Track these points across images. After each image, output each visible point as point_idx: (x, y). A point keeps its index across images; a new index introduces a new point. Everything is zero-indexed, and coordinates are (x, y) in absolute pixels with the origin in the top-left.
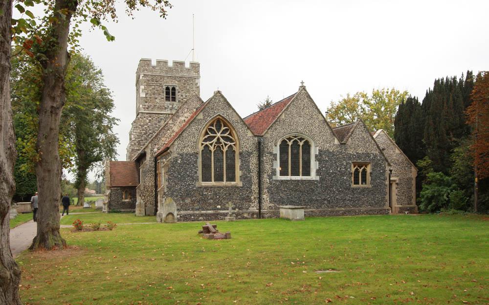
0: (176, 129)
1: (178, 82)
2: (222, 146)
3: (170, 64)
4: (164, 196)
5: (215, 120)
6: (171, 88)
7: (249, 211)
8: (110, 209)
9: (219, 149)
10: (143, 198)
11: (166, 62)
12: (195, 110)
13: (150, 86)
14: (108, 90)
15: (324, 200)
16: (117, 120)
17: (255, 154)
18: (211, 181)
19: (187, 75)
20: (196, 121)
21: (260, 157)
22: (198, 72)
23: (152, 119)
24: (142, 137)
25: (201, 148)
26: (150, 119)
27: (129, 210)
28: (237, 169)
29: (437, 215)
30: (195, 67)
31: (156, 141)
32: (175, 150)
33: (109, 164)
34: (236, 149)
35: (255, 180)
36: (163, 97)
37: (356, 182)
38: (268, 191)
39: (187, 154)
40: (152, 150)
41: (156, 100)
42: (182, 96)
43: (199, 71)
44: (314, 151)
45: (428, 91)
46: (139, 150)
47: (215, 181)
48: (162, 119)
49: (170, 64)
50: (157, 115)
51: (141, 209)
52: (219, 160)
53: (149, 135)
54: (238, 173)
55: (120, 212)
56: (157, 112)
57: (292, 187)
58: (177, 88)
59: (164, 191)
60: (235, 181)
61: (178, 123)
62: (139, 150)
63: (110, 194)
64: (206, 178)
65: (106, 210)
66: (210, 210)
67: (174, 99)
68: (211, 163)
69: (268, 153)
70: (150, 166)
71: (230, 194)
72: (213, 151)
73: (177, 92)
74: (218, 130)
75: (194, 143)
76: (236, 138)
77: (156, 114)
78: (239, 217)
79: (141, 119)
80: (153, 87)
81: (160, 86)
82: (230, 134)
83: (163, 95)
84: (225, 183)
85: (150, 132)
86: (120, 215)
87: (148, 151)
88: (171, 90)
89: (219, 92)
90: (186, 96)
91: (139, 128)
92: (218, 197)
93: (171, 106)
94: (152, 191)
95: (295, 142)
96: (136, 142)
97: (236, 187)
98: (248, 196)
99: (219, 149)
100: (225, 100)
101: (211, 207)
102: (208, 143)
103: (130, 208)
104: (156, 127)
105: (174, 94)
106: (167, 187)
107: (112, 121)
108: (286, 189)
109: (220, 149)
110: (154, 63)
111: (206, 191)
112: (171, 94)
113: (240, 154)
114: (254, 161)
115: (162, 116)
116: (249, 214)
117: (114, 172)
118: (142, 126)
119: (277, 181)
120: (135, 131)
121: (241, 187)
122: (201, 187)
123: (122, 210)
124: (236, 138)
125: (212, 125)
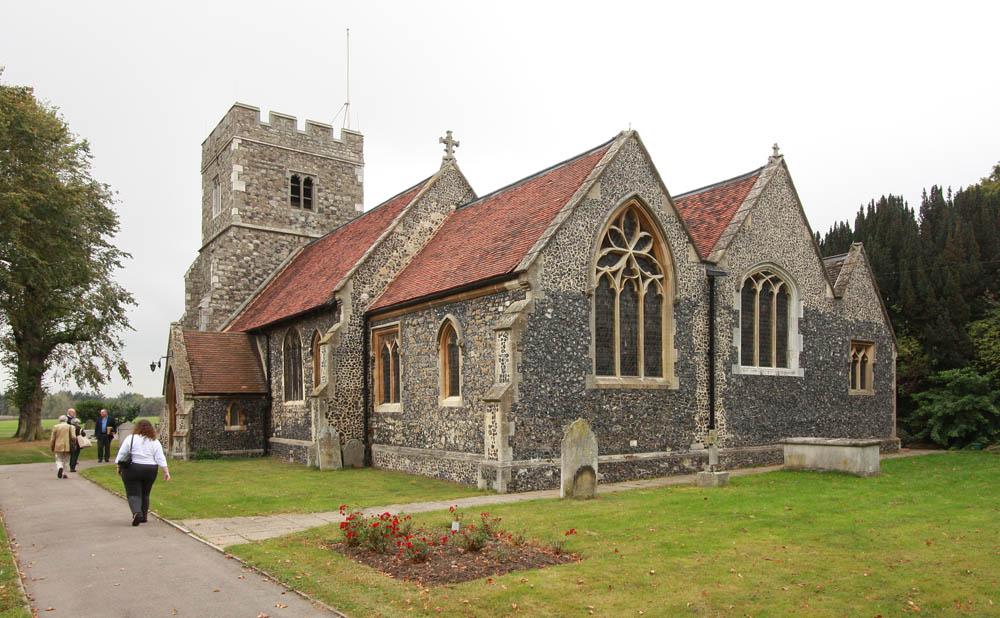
0: (412, 248)
1: (318, 167)
2: (637, 280)
3: (301, 127)
4: (513, 415)
5: (623, 212)
6: (303, 178)
7: (692, 452)
8: (192, 449)
9: (630, 287)
10: (335, 421)
11: (292, 121)
12: (453, 207)
13: (258, 167)
14: (106, 186)
15: (812, 422)
16: (124, 255)
17: (702, 308)
18: (612, 374)
19: (337, 155)
20: (586, 204)
21: (711, 315)
22: (359, 152)
23: (262, 243)
24: (237, 281)
25: (596, 279)
26: (258, 242)
27: (241, 451)
28: (668, 344)
29: (970, 456)
30: (354, 140)
31: (366, 274)
32: (539, 281)
33: (182, 337)
34: (667, 293)
35: (702, 375)
36: (285, 196)
37: (854, 387)
38: (724, 403)
39: (566, 297)
40: (354, 298)
41: (271, 202)
42: (326, 199)
43: (361, 151)
44: (795, 311)
45: (866, 212)
46: (230, 311)
47: (622, 374)
48: (283, 245)
49: (301, 127)
50: (272, 235)
51: (332, 451)
52: (629, 318)
53: (254, 279)
54: (670, 355)
55: (218, 457)
56: (273, 229)
57: (763, 391)
58: (316, 181)
59: (513, 399)
60: (661, 376)
61: (416, 234)
62: (230, 311)
63: (194, 412)
64: (605, 368)
65: (184, 454)
66: (617, 453)
67: (308, 205)
68: (613, 325)
69: (723, 308)
70: (352, 340)
71: (656, 410)
72: (619, 291)
73: (315, 189)
74: (630, 234)
75: (583, 264)
76: (668, 262)
77: (271, 232)
78: (675, 469)
79: (235, 241)
80: (264, 171)
81: (279, 172)
82: (652, 252)
83: (286, 193)
84: (642, 380)
85: (257, 271)
86: (216, 463)
87: (346, 298)
88: (302, 183)
89: (635, 135)
90: (335, 201)
91: (232, 261)
92: (631, 417)
93: (303, 219)
94: (356, 403)
95: (766, 285)
96: (224, 292)
97: (665, 391)
98: (689, 415)
99: (630, 287)
100: (647, 158)
101: (617, 446)
102: (607, 269)
103: (243, 446)
104: (272, 262)
105: (308, 193)
106: (521, 390)
107: (110, 258)
108: (753, 398)
109: (632, 290)
110: (265, 118)
111: (608, 402)
112: (302, 192)
113: (676, 304)
114: (700, 324)
115: (284, 238)
116: (693, 459)
117: (199, 358)
118: (239, 258)
119: (739, 377)
120: (221, 267)
121: (675, 391)
122: (596, 391)
123: (226, 452)
124: (668, 262)
125: (617, 223)
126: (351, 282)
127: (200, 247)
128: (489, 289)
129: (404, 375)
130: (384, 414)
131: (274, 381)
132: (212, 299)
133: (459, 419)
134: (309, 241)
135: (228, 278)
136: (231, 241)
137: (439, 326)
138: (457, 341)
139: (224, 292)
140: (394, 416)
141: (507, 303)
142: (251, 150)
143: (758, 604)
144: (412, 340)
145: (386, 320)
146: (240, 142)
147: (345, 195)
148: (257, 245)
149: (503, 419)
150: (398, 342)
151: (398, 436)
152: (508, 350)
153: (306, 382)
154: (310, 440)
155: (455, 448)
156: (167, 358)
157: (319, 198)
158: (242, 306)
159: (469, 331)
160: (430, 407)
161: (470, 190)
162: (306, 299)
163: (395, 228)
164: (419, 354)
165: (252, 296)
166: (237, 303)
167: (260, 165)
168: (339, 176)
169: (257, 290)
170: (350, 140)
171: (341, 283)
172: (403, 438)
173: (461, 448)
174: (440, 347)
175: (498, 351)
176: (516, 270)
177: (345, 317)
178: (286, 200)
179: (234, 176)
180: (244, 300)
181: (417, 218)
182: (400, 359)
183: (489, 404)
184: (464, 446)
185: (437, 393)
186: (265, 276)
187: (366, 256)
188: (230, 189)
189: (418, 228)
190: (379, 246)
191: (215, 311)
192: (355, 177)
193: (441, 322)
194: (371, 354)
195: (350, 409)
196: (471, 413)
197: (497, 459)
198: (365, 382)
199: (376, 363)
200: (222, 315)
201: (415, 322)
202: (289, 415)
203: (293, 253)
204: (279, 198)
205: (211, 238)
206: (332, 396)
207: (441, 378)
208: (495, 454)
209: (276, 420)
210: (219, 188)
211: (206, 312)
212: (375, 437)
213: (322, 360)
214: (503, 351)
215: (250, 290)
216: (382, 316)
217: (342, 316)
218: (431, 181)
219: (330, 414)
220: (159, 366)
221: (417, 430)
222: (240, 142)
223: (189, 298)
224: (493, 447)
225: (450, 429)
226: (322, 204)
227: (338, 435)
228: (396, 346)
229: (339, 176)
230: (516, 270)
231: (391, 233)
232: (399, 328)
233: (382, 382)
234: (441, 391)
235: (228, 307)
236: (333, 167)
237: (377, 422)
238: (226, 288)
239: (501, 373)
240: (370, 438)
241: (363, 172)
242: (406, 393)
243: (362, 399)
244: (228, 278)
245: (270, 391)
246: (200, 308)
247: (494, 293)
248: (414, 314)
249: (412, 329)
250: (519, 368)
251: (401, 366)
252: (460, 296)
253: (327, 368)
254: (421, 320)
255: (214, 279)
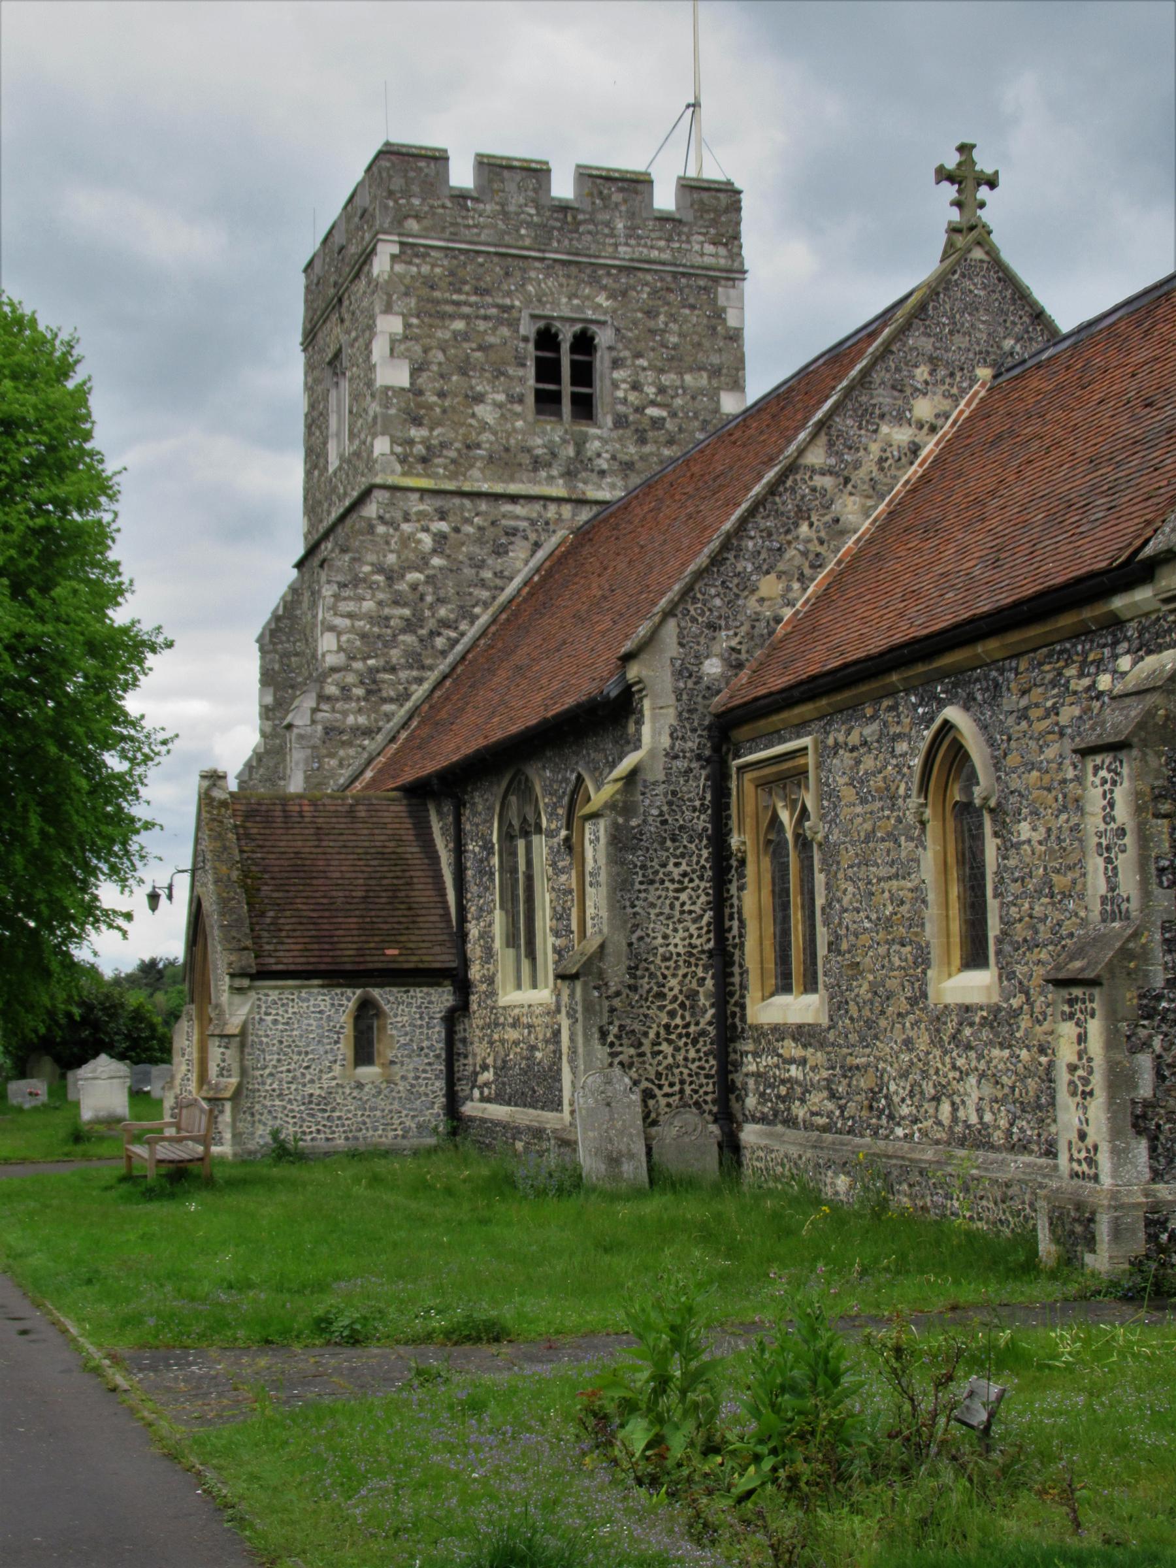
1: (612, 296)
3: (563, 188)
6: (566, 336)
19: (666, 256)
22: (731, 239)
26: (443, 526)
41: (479, 410)
43: (736, 237)
46: (368, 732)
48: (512, 532)
49: (563, 188)
50: (483, 506)
53: (433, 634)
56: (485, 487)
58: (604, 338)
62: (368, 732)
67: (584, 407)
73: (601, 361)
79: (381, 529)
80: (459, 325)
81: (500, 322)
85: (442, 612)
88: (565, 347)
90: (662, 390)
94: (693, 995)
104: (483, 584)
105: (583, 374)
110: (462, 175)
126: (672, 624)
127: (299, 551)
128: (1067, 620)
129: (829, 904)
130: (775, 1028)
131: (473, 930)
132: (322, 698)
133: (991, 1043)
134: (585, 515)
135: (364, 636)
136: (371, 529)
137: (923, 746)
138: (977, 790)
139: (351, 678)
140: (803, 1034)
141: (1125, 663)
142: (426, 269)
143: (683, 1495)
144: (848, 794)
145: (777, 736)
146: (396, 249)
147: (691, 370)
148: (440, 538)
149: (1111, 1043)
150: (810, 801)
151: (817, 1099)
152: (1122, 813)
153: (557, 934)
154: (557, 1106)
155: (977, 1139)
156: (194, 871)
157: (615, 385)
158: (403, 712)
159: (1013, 760)
160: (904, 1006)
161: (1039, 316)
162: (556, 685)
163: (801, 452)
164: (869, 837)
165: (426, 686)
166: (388, 708)
167: (449, 309)
168: (673, 317)
169: (443, 666)
170: (702, 209)
171: (643, 630)
172: (830, 1105)
173: (998, 1137)
174: (928, 813)
175: (1094, 822)
176: (1141, 556)
177: (655, 733)
178: (521, 400)
179: (380, 348)
180: (407, 695)
181: (869, 418)
182: (817, 856)
183: (1064, 993)
184: (1009, 1134)
185: (922, 959)
186: (463, 626)
187: (715, 545)
188: (370, 383)
189: (875, 448)
190: (752, 512)
191: (328, 731)
192: (719, 314)
193: (928, 734)
194: (735, 841)
195: (672, 1014)
196: (1025, 1022)
197: (1096, 1178)
198: (719, 928)
199: (750, 870)
200: (349, 744)
201: (854, 739)
202: (512, 1035)
203: (541, 554)
204: (501, 397)
205: (326, 524)
206: (616, 973)
207: (932, 912)
208: (1091, 1162)
209: (480, 1050)
210: (345, 385)
211: (301, 737)
212: (751, 1101)
213: (590, 865)
214: (1109, 818)
215: (423, 667)
216: (763, 724)
217: (646, 730)
218: (900, 313)
219: (614, 1030)
220: (170, 897)
221: (864, 1082)
222: (396, 249)
223: (269, 700)
224: (1082, 1136)
225: (963, 1075)
226: (625, 401)
227: (636, 1097)
228: (804, 814)
229: (673, 317)
230: (1141, 556)
231: (792, 468)
232: (811, 760)
233: (769, 929)
234: (935, 954)
235: (362, 720)
236: (654, 293)
237: (756, 1054)
238: (358, 665)
239: (1103, 888)
240: (735, 1106)
241: (741, 298)
242: (836, 959)
243: (709, 983)
244: (364, 636)
245: (465, 963)
246: (289, 727)
247: (1082, 633)
248: (851, 710)
249: (846, 758)
250: (1162, 871)
251: (820, 879)
252: (980, 649)
253: (603, 890)
254: (871, 730)
255: (327, 643)
